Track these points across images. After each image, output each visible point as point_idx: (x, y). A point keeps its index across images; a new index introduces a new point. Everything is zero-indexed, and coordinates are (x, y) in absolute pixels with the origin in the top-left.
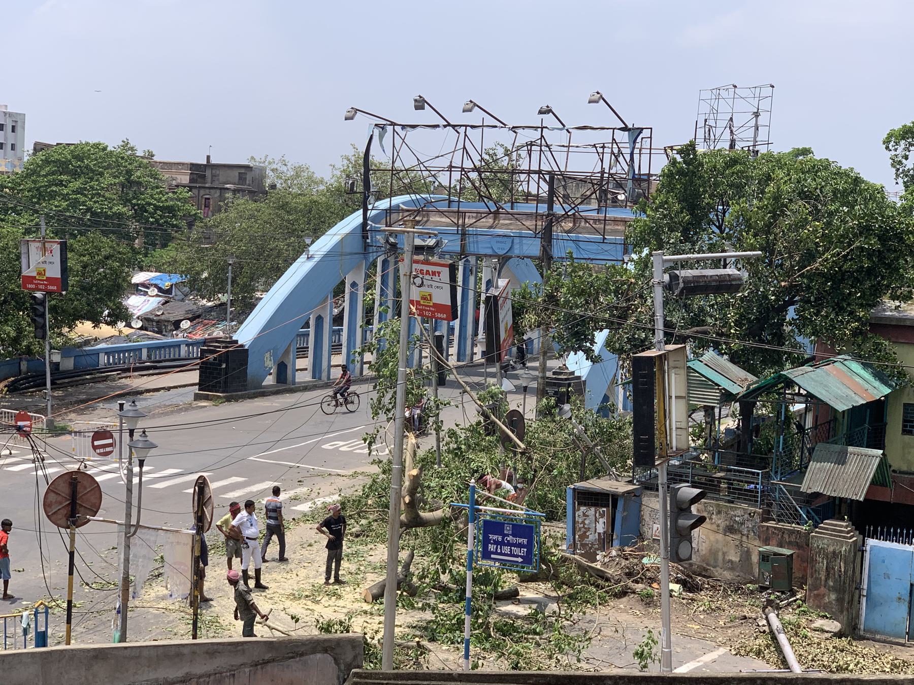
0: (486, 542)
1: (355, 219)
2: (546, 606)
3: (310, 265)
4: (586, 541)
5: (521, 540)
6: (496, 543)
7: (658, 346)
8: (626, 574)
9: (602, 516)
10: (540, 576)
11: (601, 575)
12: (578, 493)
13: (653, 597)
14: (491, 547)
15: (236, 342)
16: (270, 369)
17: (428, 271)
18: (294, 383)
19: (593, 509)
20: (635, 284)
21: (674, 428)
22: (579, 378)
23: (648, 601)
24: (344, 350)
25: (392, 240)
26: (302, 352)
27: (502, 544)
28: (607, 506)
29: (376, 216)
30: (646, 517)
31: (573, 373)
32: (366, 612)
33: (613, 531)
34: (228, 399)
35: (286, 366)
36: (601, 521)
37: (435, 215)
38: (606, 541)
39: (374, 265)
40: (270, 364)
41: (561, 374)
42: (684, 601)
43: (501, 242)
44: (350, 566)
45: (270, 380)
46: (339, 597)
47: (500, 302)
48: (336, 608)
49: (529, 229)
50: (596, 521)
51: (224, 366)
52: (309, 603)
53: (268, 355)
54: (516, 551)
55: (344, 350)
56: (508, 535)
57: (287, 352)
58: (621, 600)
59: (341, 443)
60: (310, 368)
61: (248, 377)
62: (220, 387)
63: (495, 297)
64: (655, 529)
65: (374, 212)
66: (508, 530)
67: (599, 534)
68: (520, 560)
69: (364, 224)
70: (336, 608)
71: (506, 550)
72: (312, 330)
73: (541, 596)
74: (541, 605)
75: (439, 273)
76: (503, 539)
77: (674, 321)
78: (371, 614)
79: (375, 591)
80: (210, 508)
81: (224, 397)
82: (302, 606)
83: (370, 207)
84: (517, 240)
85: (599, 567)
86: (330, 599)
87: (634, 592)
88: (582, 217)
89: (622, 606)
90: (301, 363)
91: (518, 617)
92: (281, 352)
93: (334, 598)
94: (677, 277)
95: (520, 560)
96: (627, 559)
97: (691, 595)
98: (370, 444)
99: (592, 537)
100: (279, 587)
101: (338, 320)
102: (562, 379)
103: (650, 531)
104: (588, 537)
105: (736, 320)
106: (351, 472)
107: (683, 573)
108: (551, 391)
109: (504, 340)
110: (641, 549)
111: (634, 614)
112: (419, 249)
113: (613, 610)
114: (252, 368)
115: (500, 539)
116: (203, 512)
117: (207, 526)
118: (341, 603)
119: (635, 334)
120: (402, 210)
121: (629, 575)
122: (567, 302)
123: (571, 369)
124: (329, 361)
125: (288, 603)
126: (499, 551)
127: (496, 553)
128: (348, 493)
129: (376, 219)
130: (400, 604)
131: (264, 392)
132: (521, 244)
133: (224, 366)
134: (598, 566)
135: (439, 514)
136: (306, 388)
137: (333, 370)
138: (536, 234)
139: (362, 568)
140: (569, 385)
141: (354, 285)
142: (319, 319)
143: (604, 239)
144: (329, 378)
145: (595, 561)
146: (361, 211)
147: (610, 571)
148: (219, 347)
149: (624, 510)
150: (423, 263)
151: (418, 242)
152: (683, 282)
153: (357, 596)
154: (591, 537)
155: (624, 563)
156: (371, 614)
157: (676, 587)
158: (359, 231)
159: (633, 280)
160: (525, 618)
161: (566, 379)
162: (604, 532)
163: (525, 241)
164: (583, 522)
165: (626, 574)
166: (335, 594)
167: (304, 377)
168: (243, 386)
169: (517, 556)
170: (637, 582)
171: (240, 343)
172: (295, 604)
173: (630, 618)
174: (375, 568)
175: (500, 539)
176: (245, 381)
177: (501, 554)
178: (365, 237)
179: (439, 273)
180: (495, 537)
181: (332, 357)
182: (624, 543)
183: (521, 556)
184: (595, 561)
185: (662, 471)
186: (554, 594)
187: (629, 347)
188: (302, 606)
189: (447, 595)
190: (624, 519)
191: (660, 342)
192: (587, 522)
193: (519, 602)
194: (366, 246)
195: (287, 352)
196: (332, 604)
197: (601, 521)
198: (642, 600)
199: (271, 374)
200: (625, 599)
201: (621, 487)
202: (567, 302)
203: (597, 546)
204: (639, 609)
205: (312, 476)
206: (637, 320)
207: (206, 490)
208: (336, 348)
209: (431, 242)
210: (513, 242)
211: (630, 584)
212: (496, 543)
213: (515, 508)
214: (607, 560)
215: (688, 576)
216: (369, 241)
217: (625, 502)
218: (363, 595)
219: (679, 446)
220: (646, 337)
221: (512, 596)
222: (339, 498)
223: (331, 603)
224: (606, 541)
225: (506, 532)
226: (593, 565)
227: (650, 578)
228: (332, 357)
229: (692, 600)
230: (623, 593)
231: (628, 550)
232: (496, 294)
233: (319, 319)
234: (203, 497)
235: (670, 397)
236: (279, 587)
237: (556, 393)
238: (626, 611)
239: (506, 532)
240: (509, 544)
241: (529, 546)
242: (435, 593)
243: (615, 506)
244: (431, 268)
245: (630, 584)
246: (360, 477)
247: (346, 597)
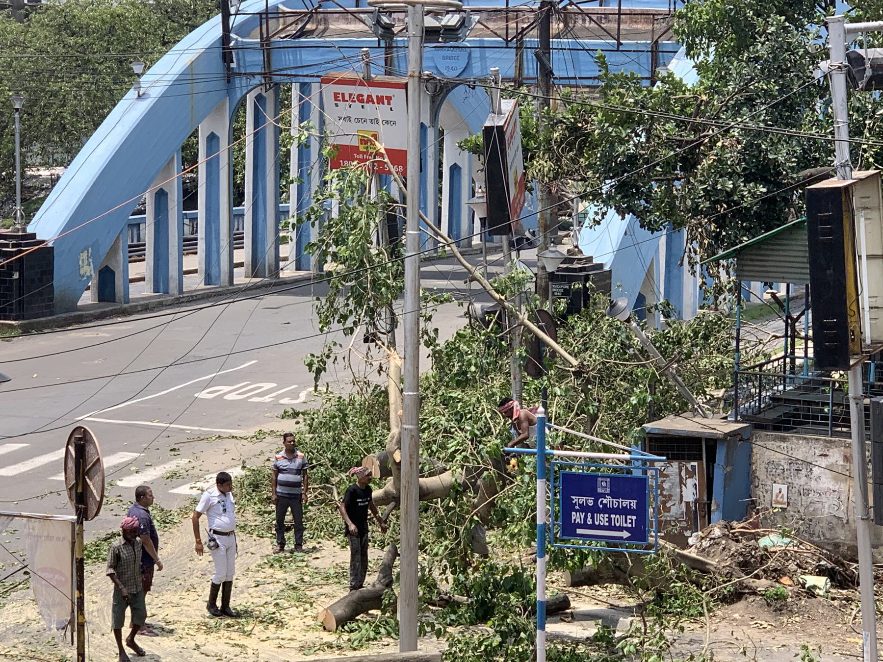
0: (568, 507)
1: (210, 31)
2: (615, 622)
3: (144, 107)
4: (665, 516)
5: (626, 503)
6: (584, 509)
7: (841, 171)
8: (739, 564)
9: (691, 474)
10: (605, 573)
11: (701, 567)
12: (650, 440)
13: (785, 598)
14: (577, 517)
15: (33, 236)
16: (89, 278)
17: (369, 96)
18: (127, 300)
19: (675, 464)
20: (707, 103)
21: (867, 309)
22: (601, 266)
23: (777, 604)
24: (201, 246)
25: (385, 19)
26: (136, 251)
27: (595, 510)
28: (699, 458)
29: (243, 24)
30: (761, 474)
31: (590, 259)
32: (330, 646)
33: (710, 498)
34: (26, 331)
35: (113, 273)
36: (690, 482)
37: (337, 20)
38: (699, 515)
39: (242, 103)
40: (89, 270)
41: (571, 261)
42: (836, 603)
43: (450, 58)
44: (286, 576)
45: (88, 298)
46: (281, 624)
47: (507, 137)
48: (282, 642)
49: (500, 36)
50: (682, 482)
51: (16, 276)
52: (234, 635)
53: (84, 255)
54: (619, 520)
55: (201, 246)
56: (603, 495)
57: (114, 250)
58: (732, 606)
59: (226, 389)
60: (149, 274)
61: (56, 292)
62: (11, 311)
63: (500, 128)
64: (776, 491)
65: (240, 19)
66: (603, 487)
67: (688, 503)
68: (625, 534)
69: (225, 39)
70: (282, 642)
71: (602, 519)
72: (149, 216)
73: (603, 607)
74: (608, 622)
75: (389, 99)
76: (596, 501)
77: (781, 159)
78: (340, 648)
79: (340, 612)
80: (97, 478)
81: (20, 326)
82: (223, 640)
83: (233, 10)
84: (476, 53)
85: (694, 555)
86: (266, 628)
87: (754, 593)
88: (582, 13)
89: (736, 616)
90: (135, 270)
91: (577, 642)
92: (104, 250)
93: (272, 627)
94: (860, 60)
95: (625, 534)
96: (737, 541)
97: (844, 592)
98: (318, 372)
99: (676, 509)
100: (180, 614)
101: (189, 199)
102: (575, 270)
103: (768, 496)
104: (668, 510)
105: (876, 153)
106: (252, 432)
107: (829, 558)
108: (556, 288)
109: (515, 199)
110: (755, 525)
111: (760, 627)
112: (431, 34)
113: (724, 623)
114: (60, 279)
115: (591, 502)
116: (86, 486)
117: (93, 508)
118: (285, 633)
119: (717, 183)
120: (284, 13)
121: (745, 566)
122: (604, 134)
123: (586, 254)
124: (126, 271)
125: (201, 638)
126: (589, 522)
127: (585, 526)
128: (255, 464)
129: (243, 30)
130: (383, 630)
131: (81, 316)
132: (483, 58)
133: (16, 276)
134: (692, 553)
135: (446, 478)
136: (146, 308)
137: (187, 279)
138: (507, 41)
139: (307, 578)
140: (587, 278)
141: (212, 138)
142: (161, 196)
143: (619, 44)
144: (181, 291)
145: (686, 546)
146: (218, 19)
147: (713, 562)
148: (7, 246)
149: (727, 464)
150: (361, 84)
151: (430, 22)
152: (872, 67)
153: (309, 621)
154: (674, 510)
155: (734, 547)
156: (340, 648)
157: (821, 581)
158: (218, 52)
159: (704, 98)
160: (589, 641)
161: (581, 270)
162: (696, 501)
163: (488, 53)
164: (660, 487)
165: (739, 564)
166: (272, 620)
167: (141, 291)
168: (47, 307)
169: (621, 529)
170: (757, 577)
171: (38, 238)
172: (212, 637)
173: (754, 633)
174: (327, 578)
175: (591, 502)
176: (51, 300)
177: (593, 527)
178: (227, 57)
179: (389, 99)
180: (582, 500)
181: (185, 258)
182: (728, 517)
183: (627, 529)
184: (686, 546)
185: (855, 377)
186: (632, 602)
187: (708, 204)
188: (223, 640)
189: (455, 613)
190: (727, 478)
191: (843, 166)
192: (666, 486)
193: (574, 617)
194: (230, 76)
195: (114, 250)
196: (272, 636)
197: (690, 482)
198: (769, 605)
199: (88, 288)
200: (740, 605)
201: (720, 425)
202: (604, 134)
203: (684, 524)
204: (765, 619)
205: (190, 440)
206: (719, 161)
207: (90, 450)
208: (189, 244)
209: (452, 20)
210: (470, 54)
211: (748, 580)
212: (584, 509)
213: (606, 449)
214: (706, 543)
215: (837, 562)
216: (233, 65)
217: (728, 447)
218: (321, 619)
219: (875, 337)
220: (735, 187)
221: (558, 609)
222: (243, 473)
223: (269, 633)
224: (699, 515)
225: (600, 490)
226: (685, 552)
227: (775, 570)
228: (185, 258)
229: (848, 599)
230: (736, 596)
231: (737, 526)
232: (501, 123)
233: (161, 196)
234: (85, 461)
235: (860, 257)
236: (180, 614)
237: (566, 293)
238: (743, 623)
239: (600, 490)
240: (606, 510)
241: (641, 512)
242: (433, 612)
243: (711, 460)
244: (376, 92)
245: (748, 580)
246: (269, 439)
247: (291, 623)
